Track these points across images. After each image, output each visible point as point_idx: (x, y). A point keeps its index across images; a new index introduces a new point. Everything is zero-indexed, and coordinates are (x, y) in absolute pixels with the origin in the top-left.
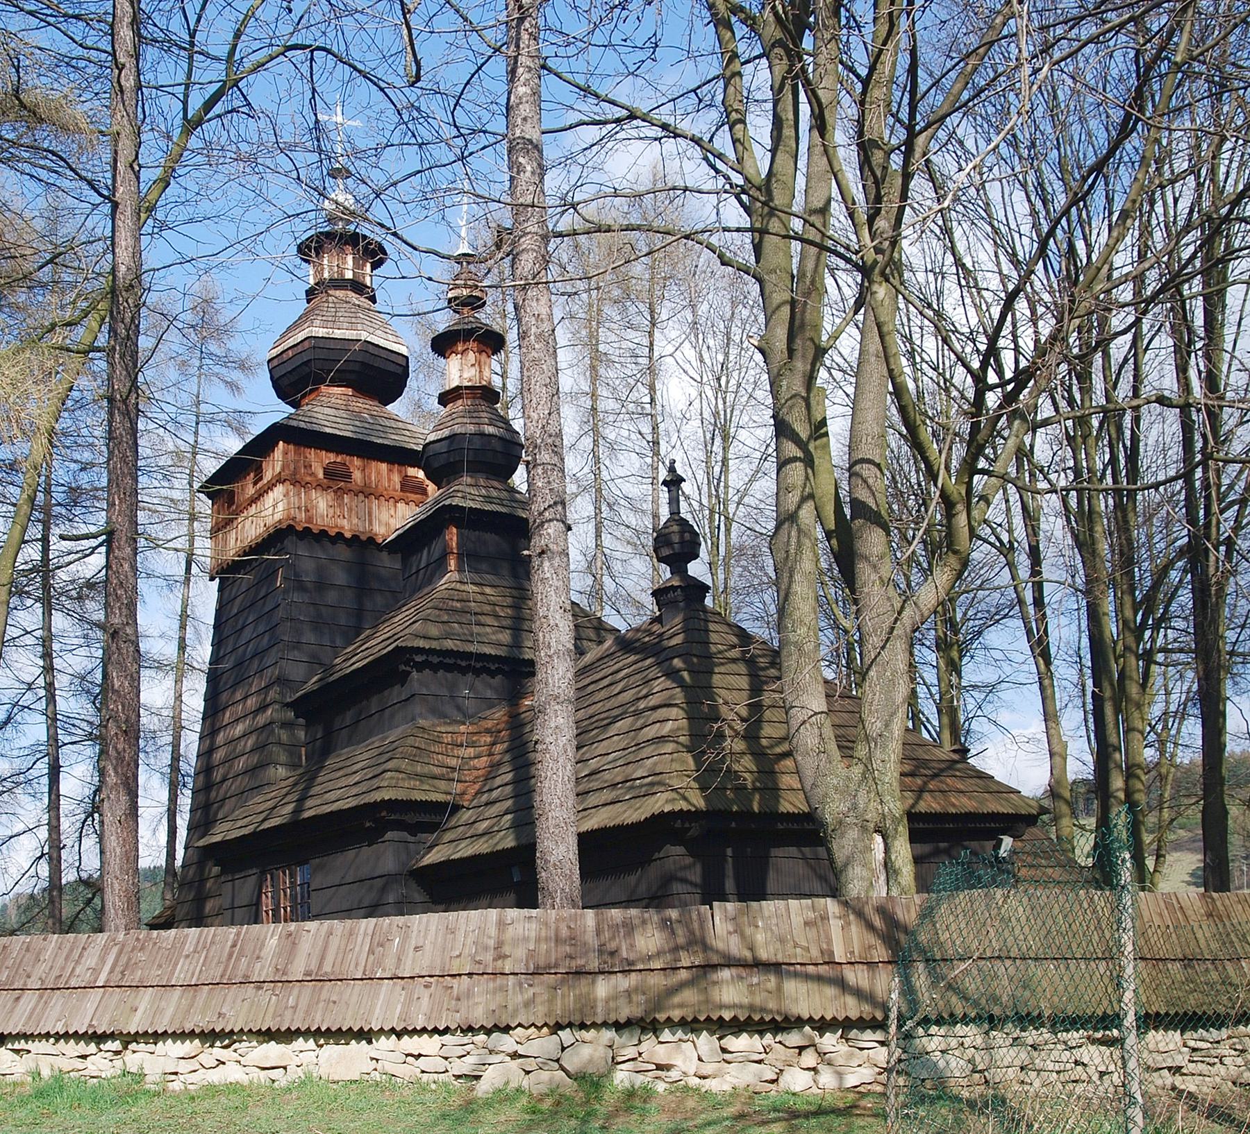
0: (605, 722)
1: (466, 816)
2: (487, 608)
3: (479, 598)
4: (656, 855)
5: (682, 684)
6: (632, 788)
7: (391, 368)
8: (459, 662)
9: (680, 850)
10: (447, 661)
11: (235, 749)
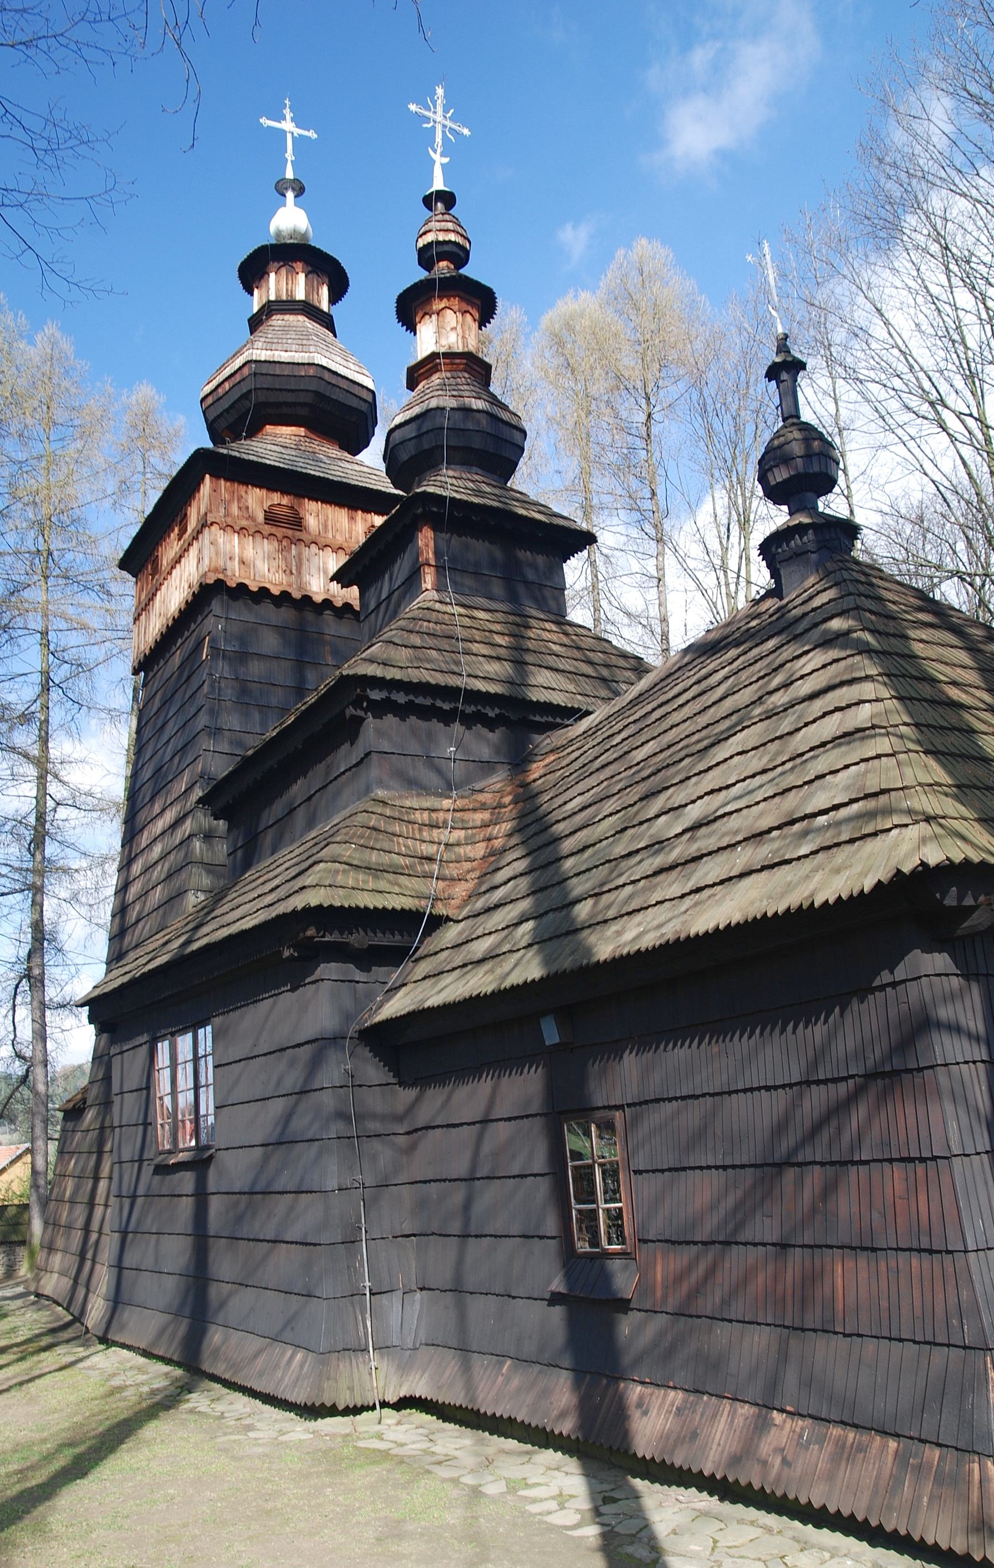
0: (705, 743)
1: (451, 934)
2: (477, 635)
3: (467, 622)
4: (886, 977)
5: (865, 650)
6: (805, 833)
7: (354, 403)
8: (439, 703)
9: (940, 961)
10: (420, 700)
11: (149, 880)
